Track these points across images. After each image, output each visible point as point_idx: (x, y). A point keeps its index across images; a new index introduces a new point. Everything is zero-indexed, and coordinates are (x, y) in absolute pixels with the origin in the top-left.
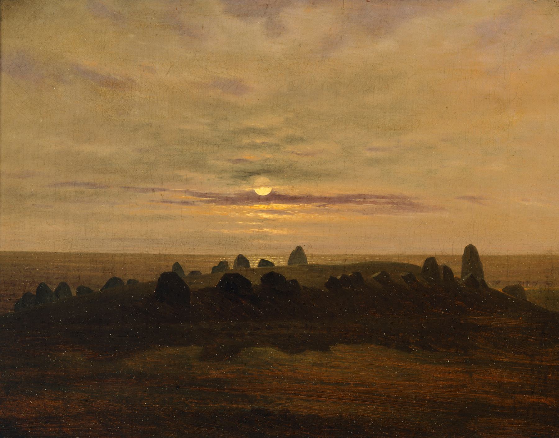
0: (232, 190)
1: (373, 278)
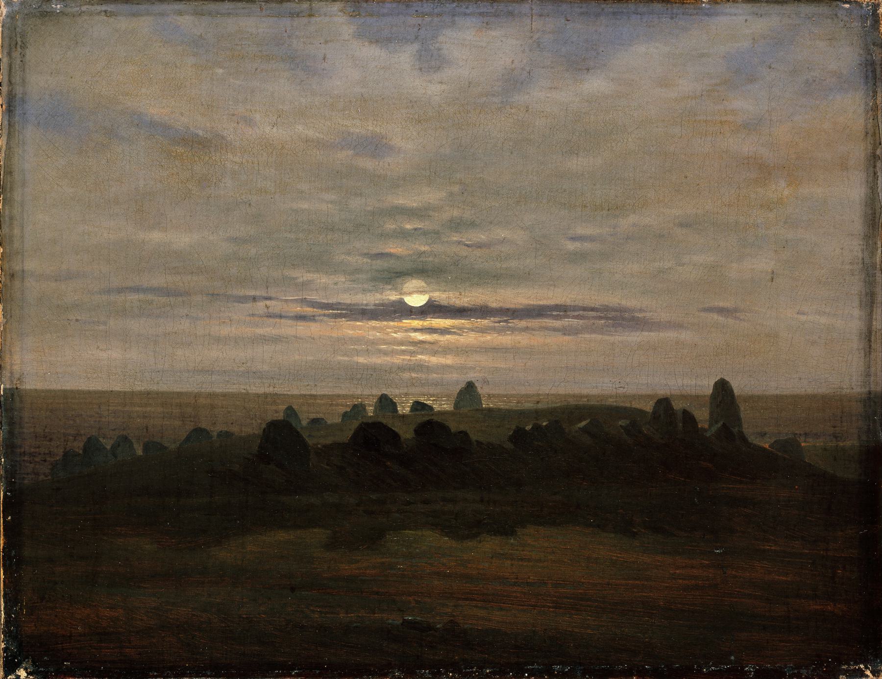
0: (371, 299)
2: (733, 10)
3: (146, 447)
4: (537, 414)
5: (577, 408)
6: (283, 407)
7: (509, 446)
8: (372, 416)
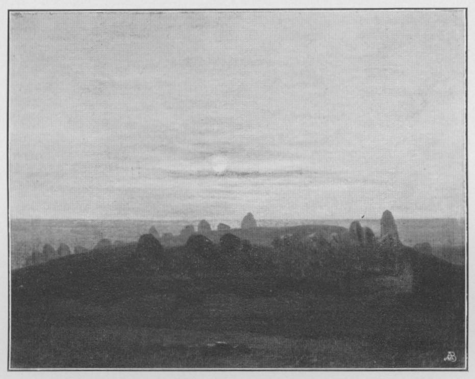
0: (195, 167)
1: (310, 238)
2: (175, 218)
3: (76, 250)
4: (287, 230)
5: (308, 226)
6: (149, 228)
7: (272, 246)
8: (443, 358)
